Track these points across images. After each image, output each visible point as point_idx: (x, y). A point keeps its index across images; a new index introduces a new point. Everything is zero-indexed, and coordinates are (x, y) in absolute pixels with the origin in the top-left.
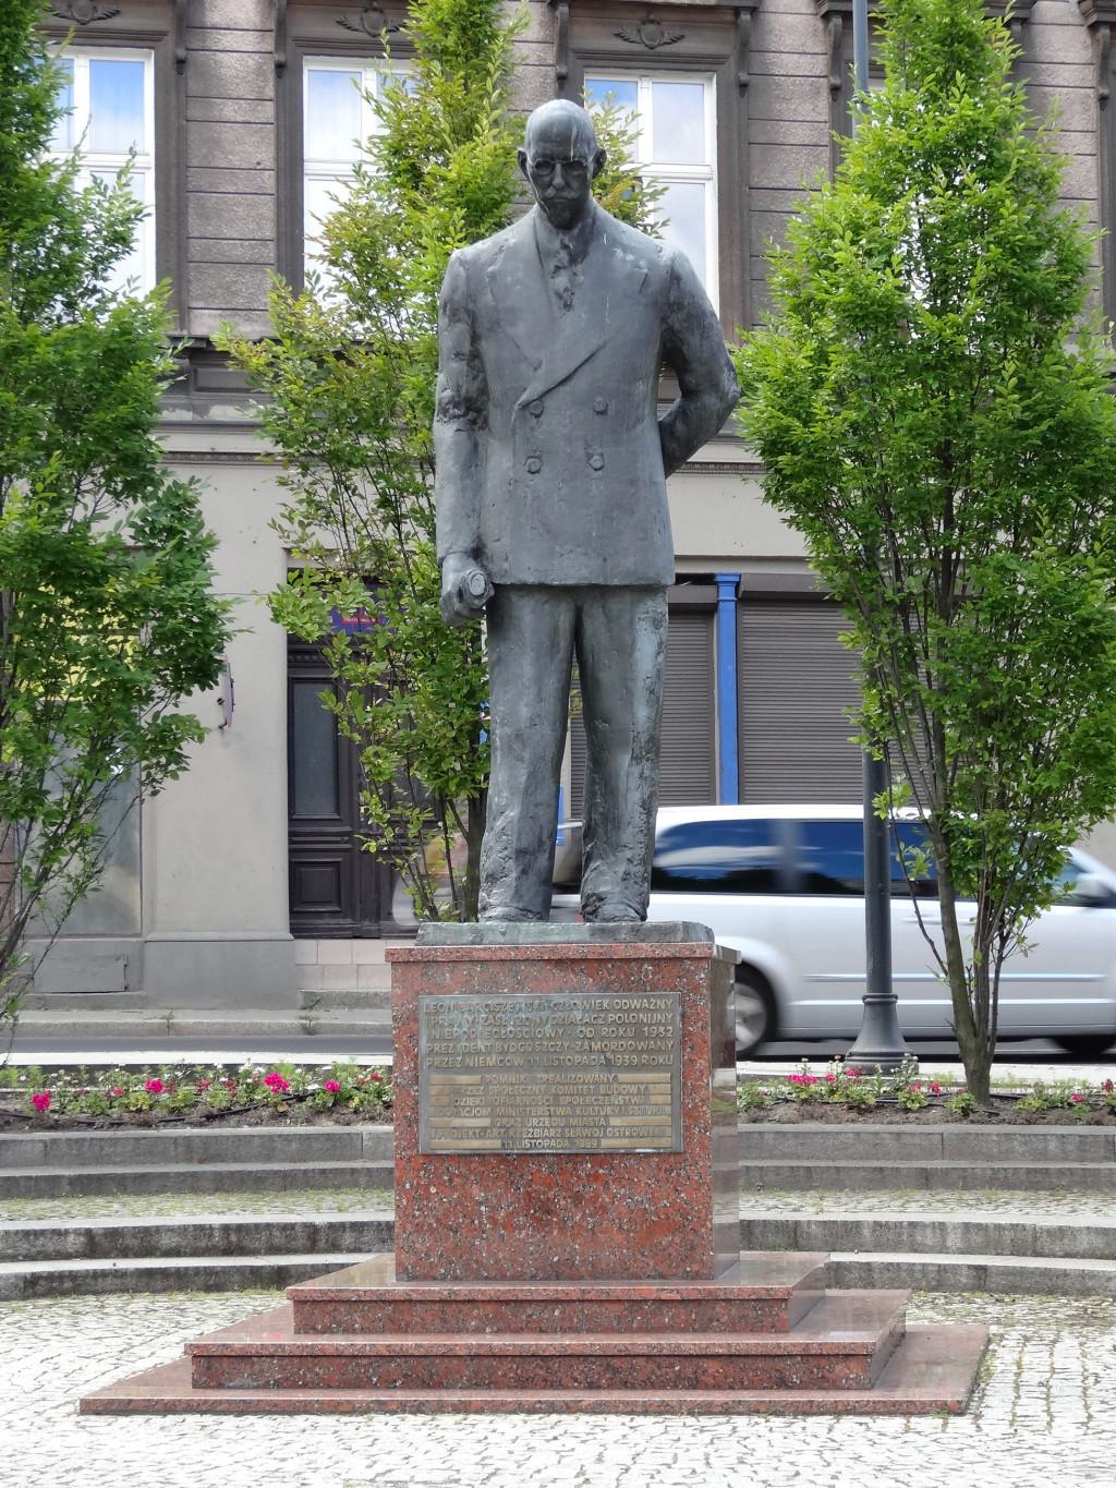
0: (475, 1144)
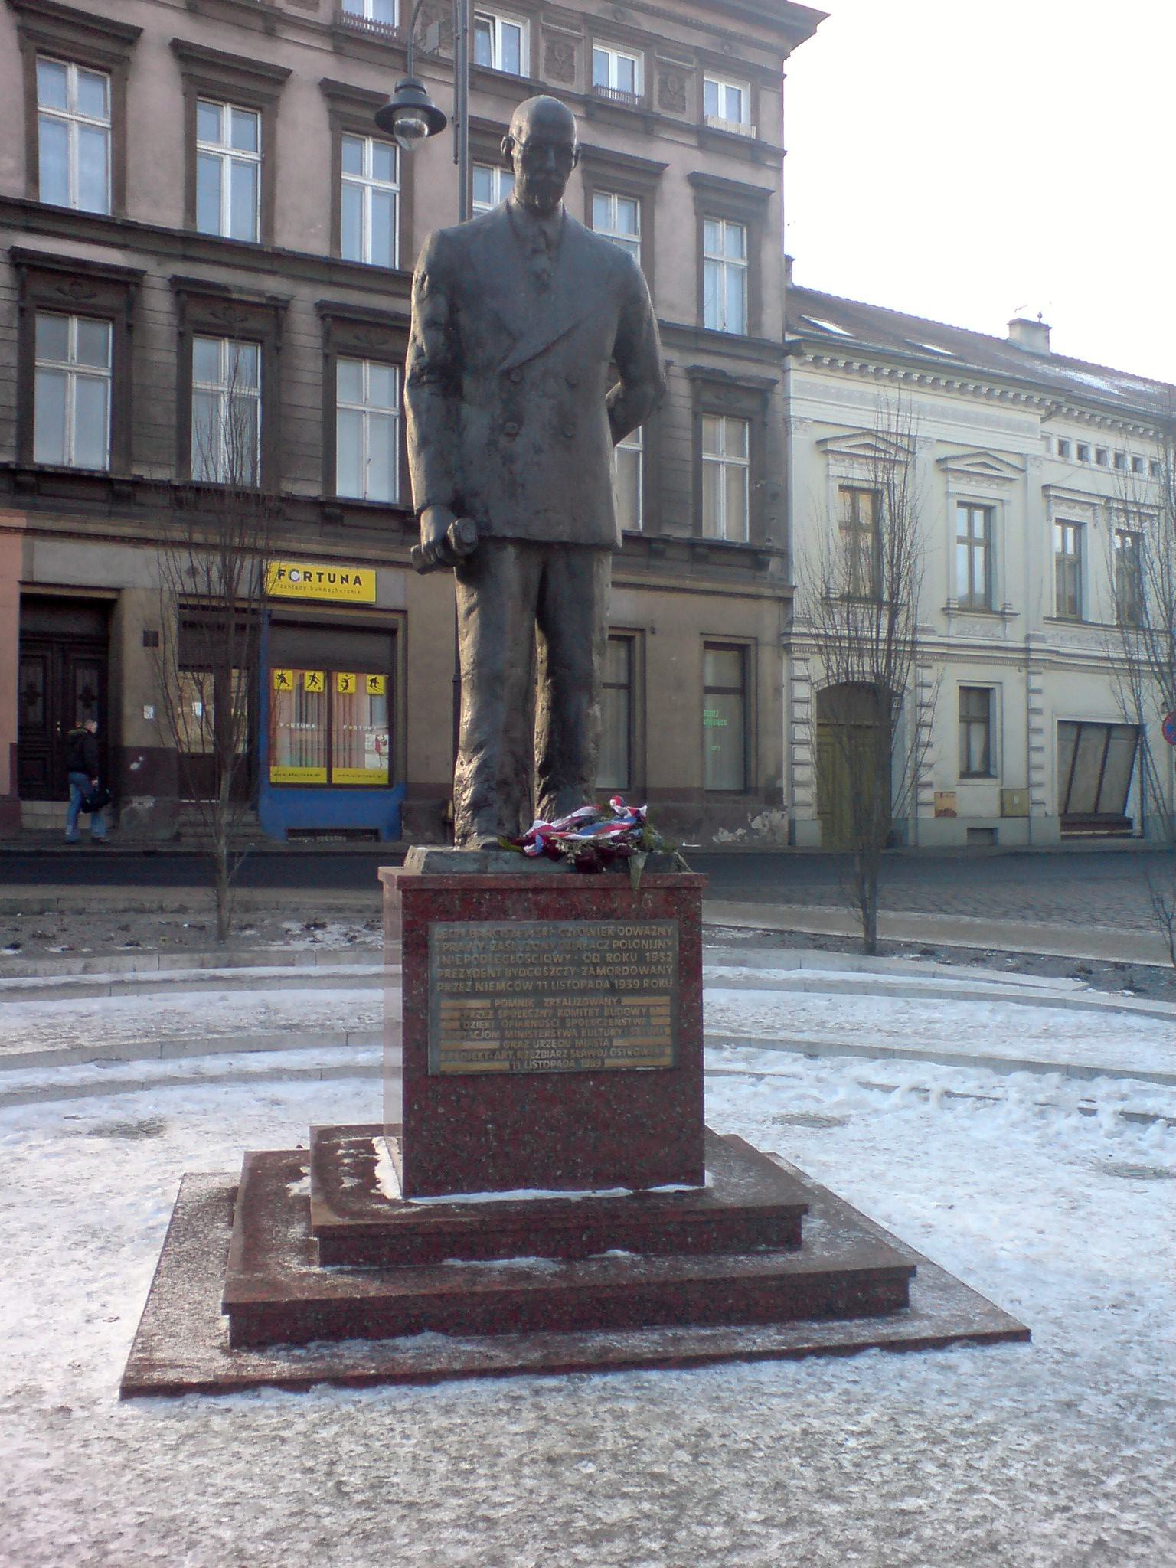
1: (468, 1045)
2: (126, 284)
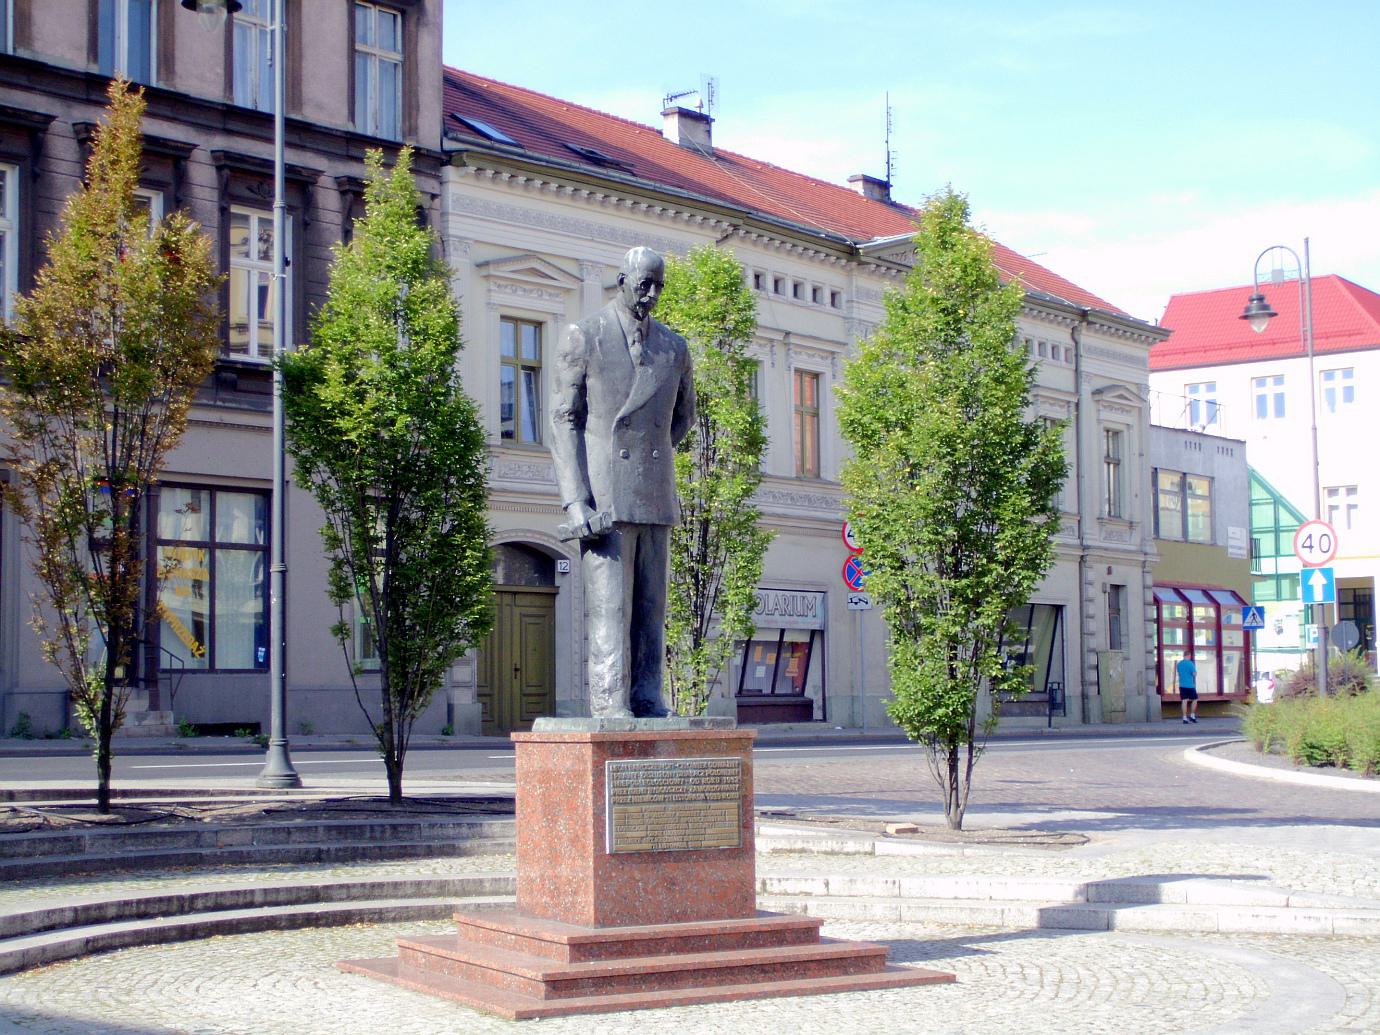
0: (638, 847)
1: (629, 834)
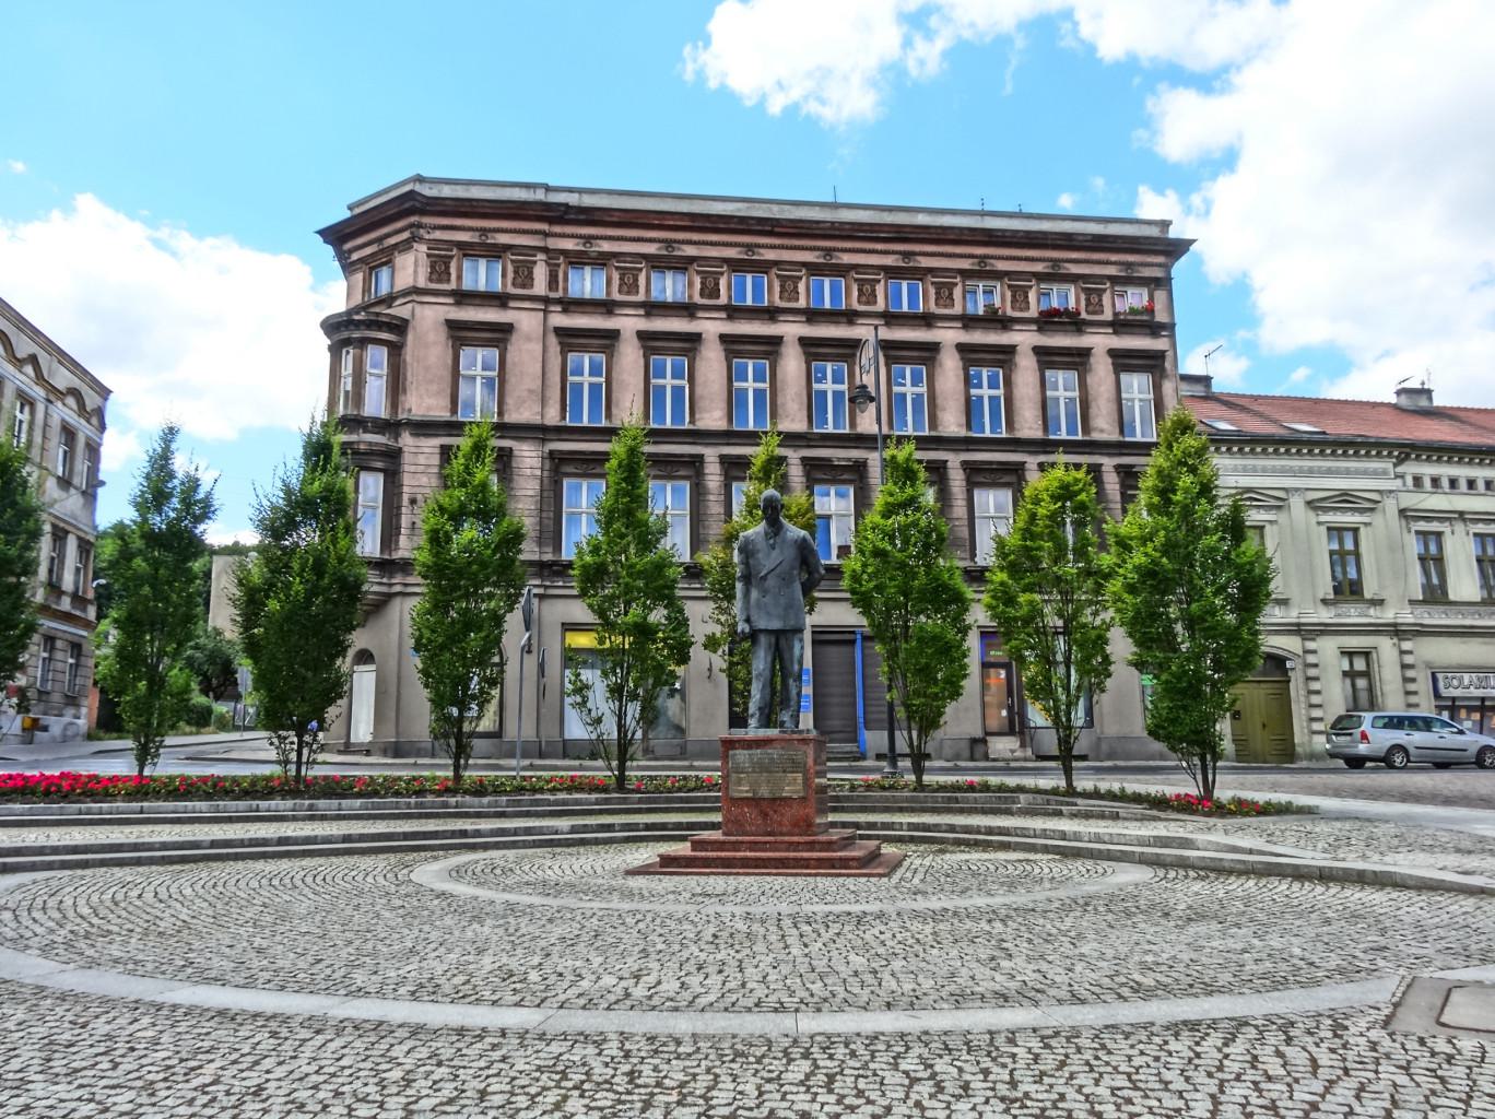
2: (1016, 470)
